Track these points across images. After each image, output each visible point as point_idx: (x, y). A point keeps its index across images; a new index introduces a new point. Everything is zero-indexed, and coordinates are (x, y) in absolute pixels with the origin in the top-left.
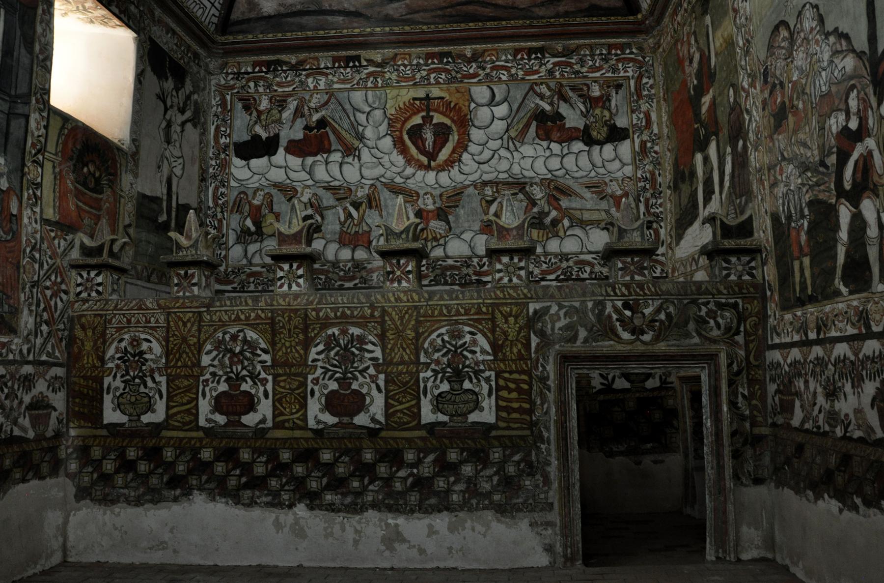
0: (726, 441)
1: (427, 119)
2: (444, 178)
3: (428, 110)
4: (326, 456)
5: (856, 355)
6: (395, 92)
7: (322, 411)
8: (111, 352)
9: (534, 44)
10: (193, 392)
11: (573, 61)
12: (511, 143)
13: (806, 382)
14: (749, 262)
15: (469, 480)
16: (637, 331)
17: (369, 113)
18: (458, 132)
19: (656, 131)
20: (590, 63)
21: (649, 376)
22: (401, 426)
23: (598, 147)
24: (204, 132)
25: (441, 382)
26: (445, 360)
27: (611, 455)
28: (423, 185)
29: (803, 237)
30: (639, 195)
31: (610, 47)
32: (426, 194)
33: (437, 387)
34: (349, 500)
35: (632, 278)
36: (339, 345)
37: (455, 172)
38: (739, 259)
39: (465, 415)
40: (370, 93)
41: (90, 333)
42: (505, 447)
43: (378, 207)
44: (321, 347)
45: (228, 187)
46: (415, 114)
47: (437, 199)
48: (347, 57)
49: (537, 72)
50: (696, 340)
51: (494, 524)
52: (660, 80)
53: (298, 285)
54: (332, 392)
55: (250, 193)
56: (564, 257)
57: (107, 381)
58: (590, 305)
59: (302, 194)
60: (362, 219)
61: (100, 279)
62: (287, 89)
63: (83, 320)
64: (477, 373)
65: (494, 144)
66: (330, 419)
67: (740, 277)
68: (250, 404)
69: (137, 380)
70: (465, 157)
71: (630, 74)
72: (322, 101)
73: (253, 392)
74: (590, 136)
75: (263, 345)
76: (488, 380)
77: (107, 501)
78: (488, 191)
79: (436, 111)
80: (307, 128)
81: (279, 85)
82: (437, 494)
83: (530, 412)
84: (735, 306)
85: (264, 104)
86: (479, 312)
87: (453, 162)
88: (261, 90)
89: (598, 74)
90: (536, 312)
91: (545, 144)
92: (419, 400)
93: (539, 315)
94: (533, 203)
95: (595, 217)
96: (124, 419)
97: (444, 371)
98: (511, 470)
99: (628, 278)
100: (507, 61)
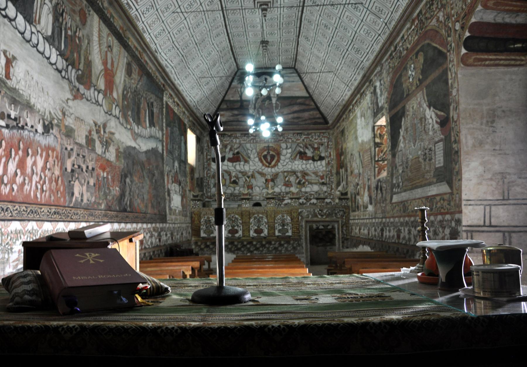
0: (341, 239)
1: (268, 153)
2: (273, 170)
4: (254, 243)
5: (24, 228)
8: (202, 220)
16: (322, 216)
21: (328, 225)
22: (271, 236)
24: (203, 156)
27: (318, 246)
31: (320, 133)
37: (276, 168)
39: (285, 234)
43: (255, 178)
50: (335, 218)
52: (334, 143)
56: (306, 193)
57: (201, 227)
60: (250, 181)
64: (288, 225)
65: (287, 161)
66: (255, 235)
68: (237, 232)
70: (279, 164)
71: (326, 141)
78: (286, 174)
80: (234, 154)
81: (225, 141)
83: (299, 233)
93: (301, 212)
94: (298, 177)
95: (315, 181)
98: (295, 245)
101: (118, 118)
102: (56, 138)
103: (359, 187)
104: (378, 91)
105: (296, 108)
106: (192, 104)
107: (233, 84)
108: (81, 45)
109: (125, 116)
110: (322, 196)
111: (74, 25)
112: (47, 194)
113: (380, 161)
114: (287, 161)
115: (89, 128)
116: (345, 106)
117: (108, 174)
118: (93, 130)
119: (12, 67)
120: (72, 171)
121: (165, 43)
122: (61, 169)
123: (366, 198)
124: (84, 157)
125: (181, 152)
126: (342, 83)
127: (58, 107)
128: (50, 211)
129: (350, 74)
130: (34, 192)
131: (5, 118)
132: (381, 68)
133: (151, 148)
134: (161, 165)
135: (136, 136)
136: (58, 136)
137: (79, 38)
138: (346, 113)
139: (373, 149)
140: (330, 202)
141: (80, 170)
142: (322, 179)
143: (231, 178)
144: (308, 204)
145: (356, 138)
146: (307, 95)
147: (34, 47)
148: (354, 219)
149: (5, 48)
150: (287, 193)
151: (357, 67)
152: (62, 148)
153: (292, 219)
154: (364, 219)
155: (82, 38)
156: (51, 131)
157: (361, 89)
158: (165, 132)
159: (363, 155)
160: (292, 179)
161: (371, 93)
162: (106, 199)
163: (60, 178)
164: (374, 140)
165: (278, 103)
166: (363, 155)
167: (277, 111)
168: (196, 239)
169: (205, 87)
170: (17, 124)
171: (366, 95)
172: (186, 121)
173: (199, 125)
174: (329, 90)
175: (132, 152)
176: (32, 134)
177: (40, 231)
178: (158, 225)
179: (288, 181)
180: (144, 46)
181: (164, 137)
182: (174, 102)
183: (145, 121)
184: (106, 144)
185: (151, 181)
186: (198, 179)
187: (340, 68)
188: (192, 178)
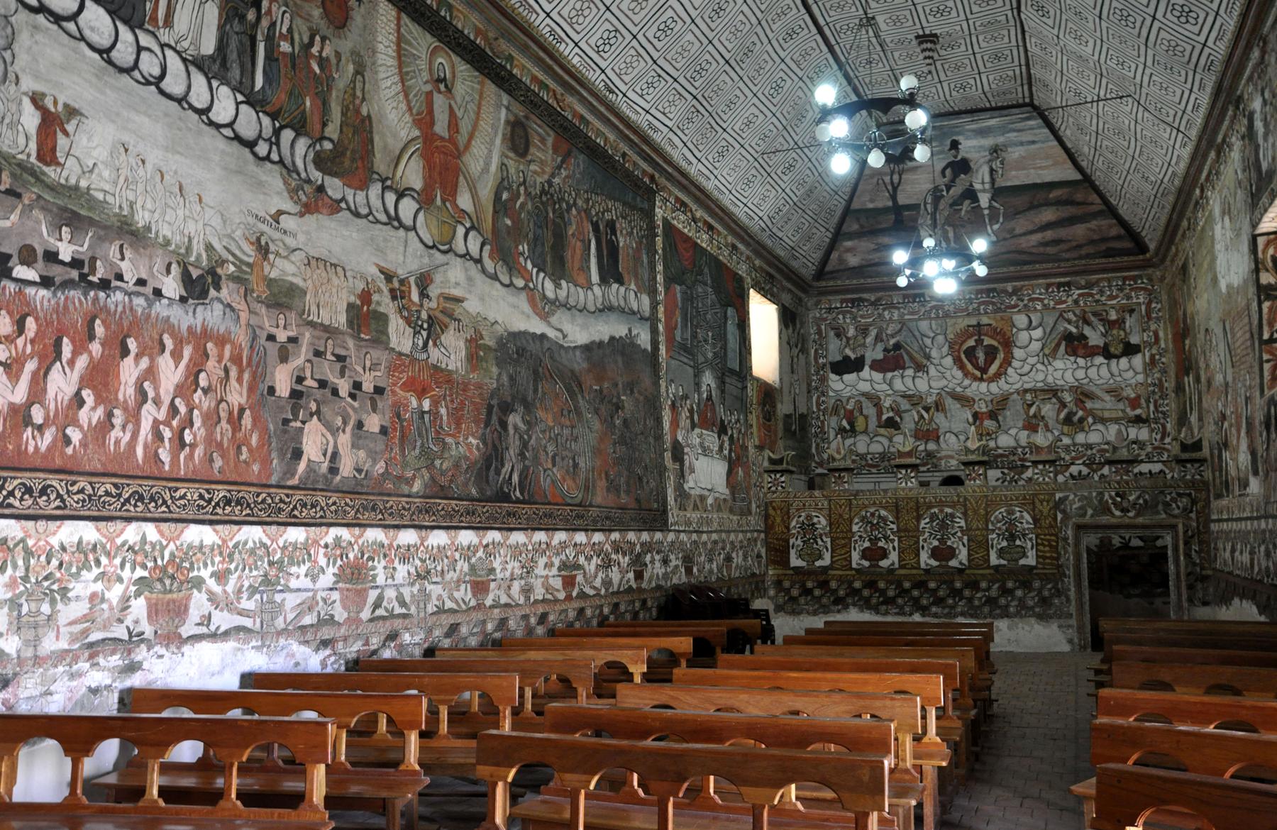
0: (1183, 577)
1: (979, 342)
2: (994, 387)
3: (980, 335)
4: (932, 585)
8: (793, 523)
9: (1062, 280)
10: (848, 547)
15: (1020, 599)
22: (978, 567)
27: (1129, 596)
31: (1125, 279)
34: (946, 611)
37: (1002, 382)
39: (1017, 560)
42: (1042, 580)
43: (944, 411)
45: (828, 396)
46: (969, 338)
49: (1065, 302)
50: (1164, 516)
51: (1036, 626)
54: (935, 547)
55: (844, 400)
56: (1089, 446)
60: (931, 420)
64: (1024, 535)
65: (1032, 360)
66: (934, 563)
68: (884, 554)
70: (1010, 370)
71: (1141, 300)
74: (1108, 351)
76: (1031, 539)
77: (794, 613)
78: (1028, 396)
80: (885, 350)
81: (862, 317)
82: (1000, 607)
83: (1058, 559)
84: (1190, 495)
85: (851, 332)
86: (1025, 498)
89: (1114, 302)
91: (1072, 359)
93: (1062, 500)
95: (1114, 415)
96: (803, 564)
98: (1046, 593)
101: (479, 261)
102: (233, 310)
103: (1226, 425)
104: (1259, 125)
105: (1048, 215)
106: (754, 226)
108: (330, 79)
109: (505, 256)
110: (1124, 454)
111: (304, 28)
112: (199, 452)
115: (361, 286)
116: (1180, 191)
117: (435, 403)
118: (379, 291)
119: (66, 134)
120: (295, 395)
121: (629, 65)
122: (251, 389)
123: (1244, 458)
124: (341, 359)
125: (724, 347)
126: (1162, 126)
127: (238, 233)
128: (207, 496)
129: (1179, 93)
130: (146, 446)
131: (35, 261)
132: (1263, 52)
133: (606, 339)
134: (647, 381)
135: (544, 307)
136: (240, 305)
137: (323, 62)
138: (1188, 214)
139: (1255, 305)
140: (1161, 471)
141: (327, 392)
142: (1134, 408)
143: (880, 413)
144: (1096, 478)
145: (1215, 281)
146: (1078, 177)
147: (148, 83)
148: (1219, 521)
149: (39, 87)
151: (1192, 65)
152: (254, 338)
153: (1036, 520)
154: (1240, 519)
155: (333, 61)
156: (213, 293)
157: (1215, 131)
158: (661, 297)
159: (1232, 329)
161: (1243, 138)
162: (430, 467)
163: (248, 412)
164: (1258, 279)
165: (995, 204)
166: (1232, 329)
167: (996, 227)
168: (780, 572)
170: (83, 277)
171: (1230, 146)
172: (742, 270)
173: (789, 279)
174: (1131, 152)
175: (533, 347)
176: (139, 302)
177: (172, 546)
178: (631, 536)
179: (1035, 416)
180: (567, 77)
181: (661, 309)
182: (694, 220)
183: (586, 269)
184: (432, 328)
185: (608, 422)
186: (788, 416)
187: (1146, 79)
188: (768, 416)
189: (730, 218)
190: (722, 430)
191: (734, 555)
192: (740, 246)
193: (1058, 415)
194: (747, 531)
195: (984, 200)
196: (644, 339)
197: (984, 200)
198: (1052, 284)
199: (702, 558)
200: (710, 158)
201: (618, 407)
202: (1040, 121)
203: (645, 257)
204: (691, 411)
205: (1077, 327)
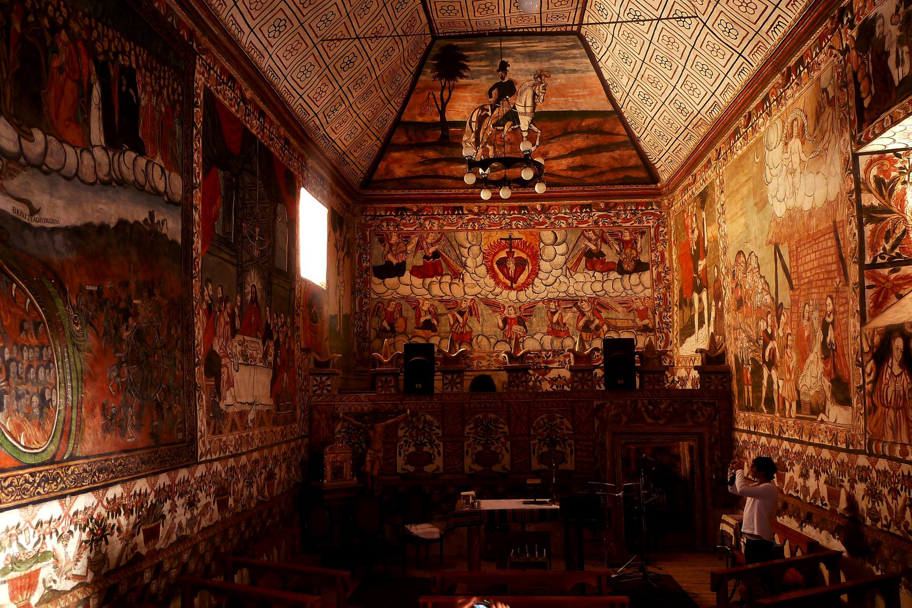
1: (511, 254)
2: (522, 296)
3: (511, 248)
6: (487, 234)
7: (473, 463)
9: (585, 202)
11: (612, 214)
12: (568, 272)
13: (750, 453)
14: (723, 378)
17: (469, 248)
18: (532, 263)
19: (668, 265)
20: (624, 216)
23: (628, 276)
25: (543, 446)
26: (545, 433)
28: (508, 300)
29: (749, 376)
30: (655, 310)
31: (637, 204)
32: (509, 307)
33: (541, 449)
35: (654, 387)
36: (483, 424)
37: (529, 291)
38: (716, 377)
40: (470, 233)
41: (324, 416)
43: (477, 315)
44: (472, 425)
47: (518, 310)
48: (454, 207)
49: (586, 222)
50: (691, 424)
53: (457, 388)
54: (479, 451)
55: (385, 302)
58: (629, 402)
59: (423, 305)
60: (465, 323)
61: (329, 382)
62: (410, 229)
63: (319, 408)
64: (564, 441)
65: (556, 273)
67: (716, 387)
68: (429, 459)
69: (356, 445)
71: (651, 224)
72: (436, 238)
73: (431, 452)
74: (622, 268)
75: (436, 424)
76: (570, 445)
78: (552, 306)
79: (517, 248)
80: (426, 257)
81: (404, 225)
84: (713, 404)
85: (394, 239)
87: (529, 284)
88: (391, 228)
89: (628, 224)
90: (598, 406)
91: (591, 273)
92: (530, 456)
94: (583, 314)
97: (545, 440)
99: (651, 387)
100: (565, 214)
105: (579, 142)
107: (422, 78)
113: (883, 266)
114: (556, 273)
133: (113, 222)
142: (642, 319)
150: (556, 353)
160: (569, 317)
164: (859, 200)
169: (344, 74)
179: (558, 323)
181: (198, 194)
182: (244, 99)
189: (284, 106)
190: (267, 335)
191: (277, 471)
192: (292, 141)
193: (578, 322)
194: (290, 441)
195: (524, 123)
196: (172, 227)
197: (524, 123)
198: (576, 205)
199: (240, 485)
200: (265, 29)
201: (127, 313)
202: (584, 50)
203: (178, 128)
204: (232, 316)
205: (596, 245)
